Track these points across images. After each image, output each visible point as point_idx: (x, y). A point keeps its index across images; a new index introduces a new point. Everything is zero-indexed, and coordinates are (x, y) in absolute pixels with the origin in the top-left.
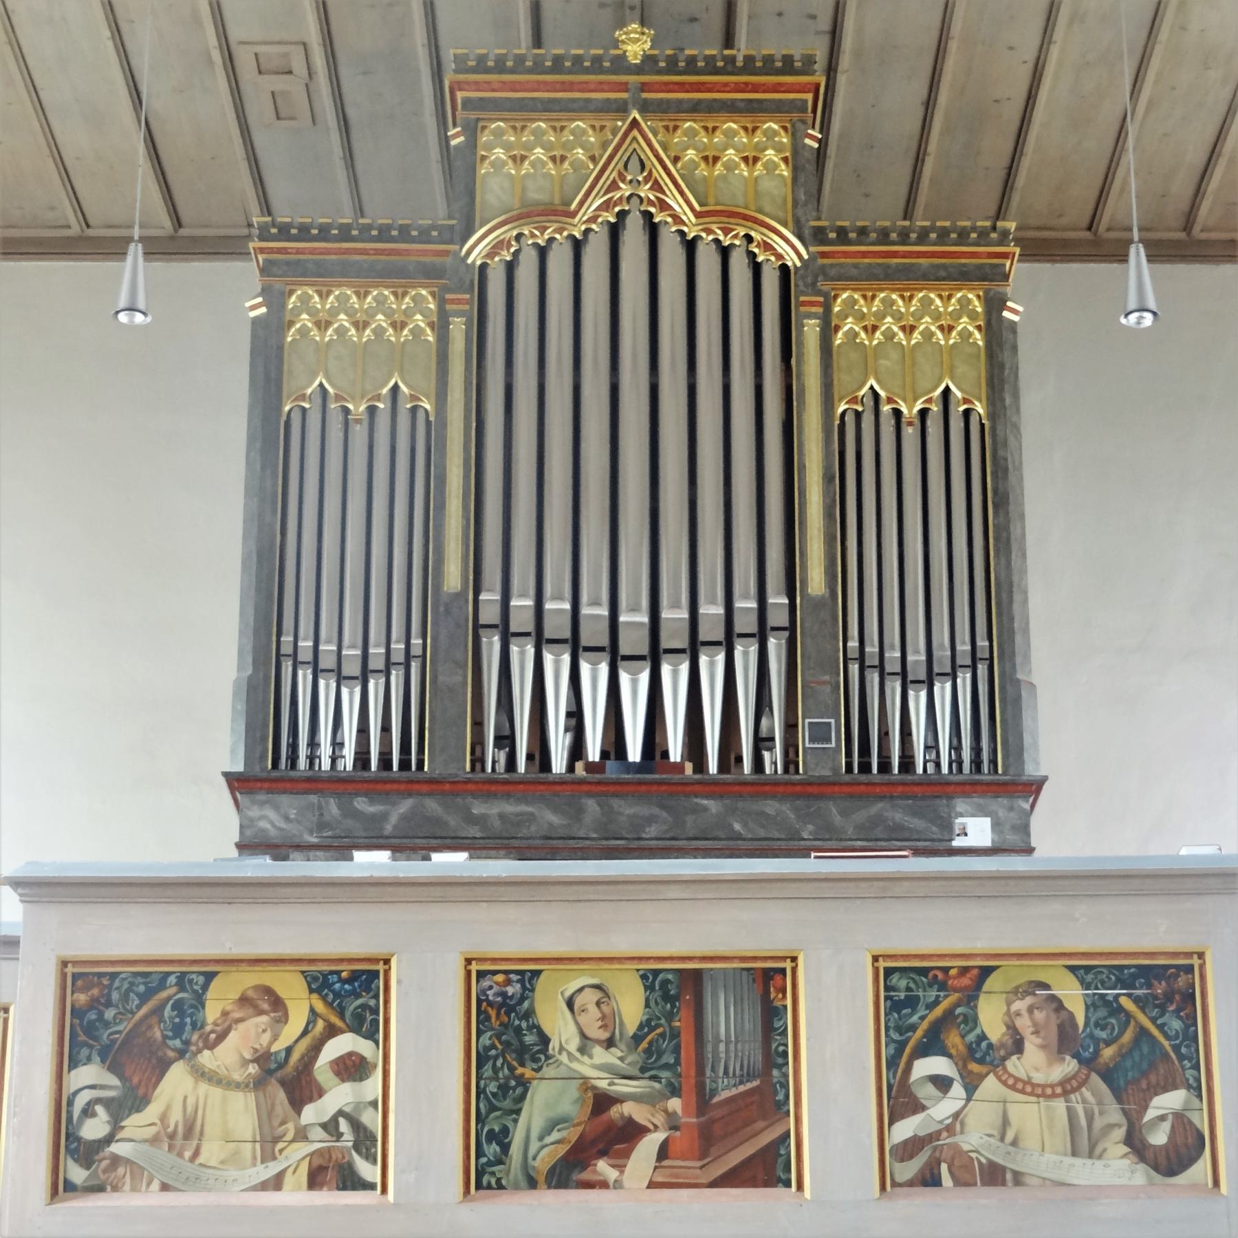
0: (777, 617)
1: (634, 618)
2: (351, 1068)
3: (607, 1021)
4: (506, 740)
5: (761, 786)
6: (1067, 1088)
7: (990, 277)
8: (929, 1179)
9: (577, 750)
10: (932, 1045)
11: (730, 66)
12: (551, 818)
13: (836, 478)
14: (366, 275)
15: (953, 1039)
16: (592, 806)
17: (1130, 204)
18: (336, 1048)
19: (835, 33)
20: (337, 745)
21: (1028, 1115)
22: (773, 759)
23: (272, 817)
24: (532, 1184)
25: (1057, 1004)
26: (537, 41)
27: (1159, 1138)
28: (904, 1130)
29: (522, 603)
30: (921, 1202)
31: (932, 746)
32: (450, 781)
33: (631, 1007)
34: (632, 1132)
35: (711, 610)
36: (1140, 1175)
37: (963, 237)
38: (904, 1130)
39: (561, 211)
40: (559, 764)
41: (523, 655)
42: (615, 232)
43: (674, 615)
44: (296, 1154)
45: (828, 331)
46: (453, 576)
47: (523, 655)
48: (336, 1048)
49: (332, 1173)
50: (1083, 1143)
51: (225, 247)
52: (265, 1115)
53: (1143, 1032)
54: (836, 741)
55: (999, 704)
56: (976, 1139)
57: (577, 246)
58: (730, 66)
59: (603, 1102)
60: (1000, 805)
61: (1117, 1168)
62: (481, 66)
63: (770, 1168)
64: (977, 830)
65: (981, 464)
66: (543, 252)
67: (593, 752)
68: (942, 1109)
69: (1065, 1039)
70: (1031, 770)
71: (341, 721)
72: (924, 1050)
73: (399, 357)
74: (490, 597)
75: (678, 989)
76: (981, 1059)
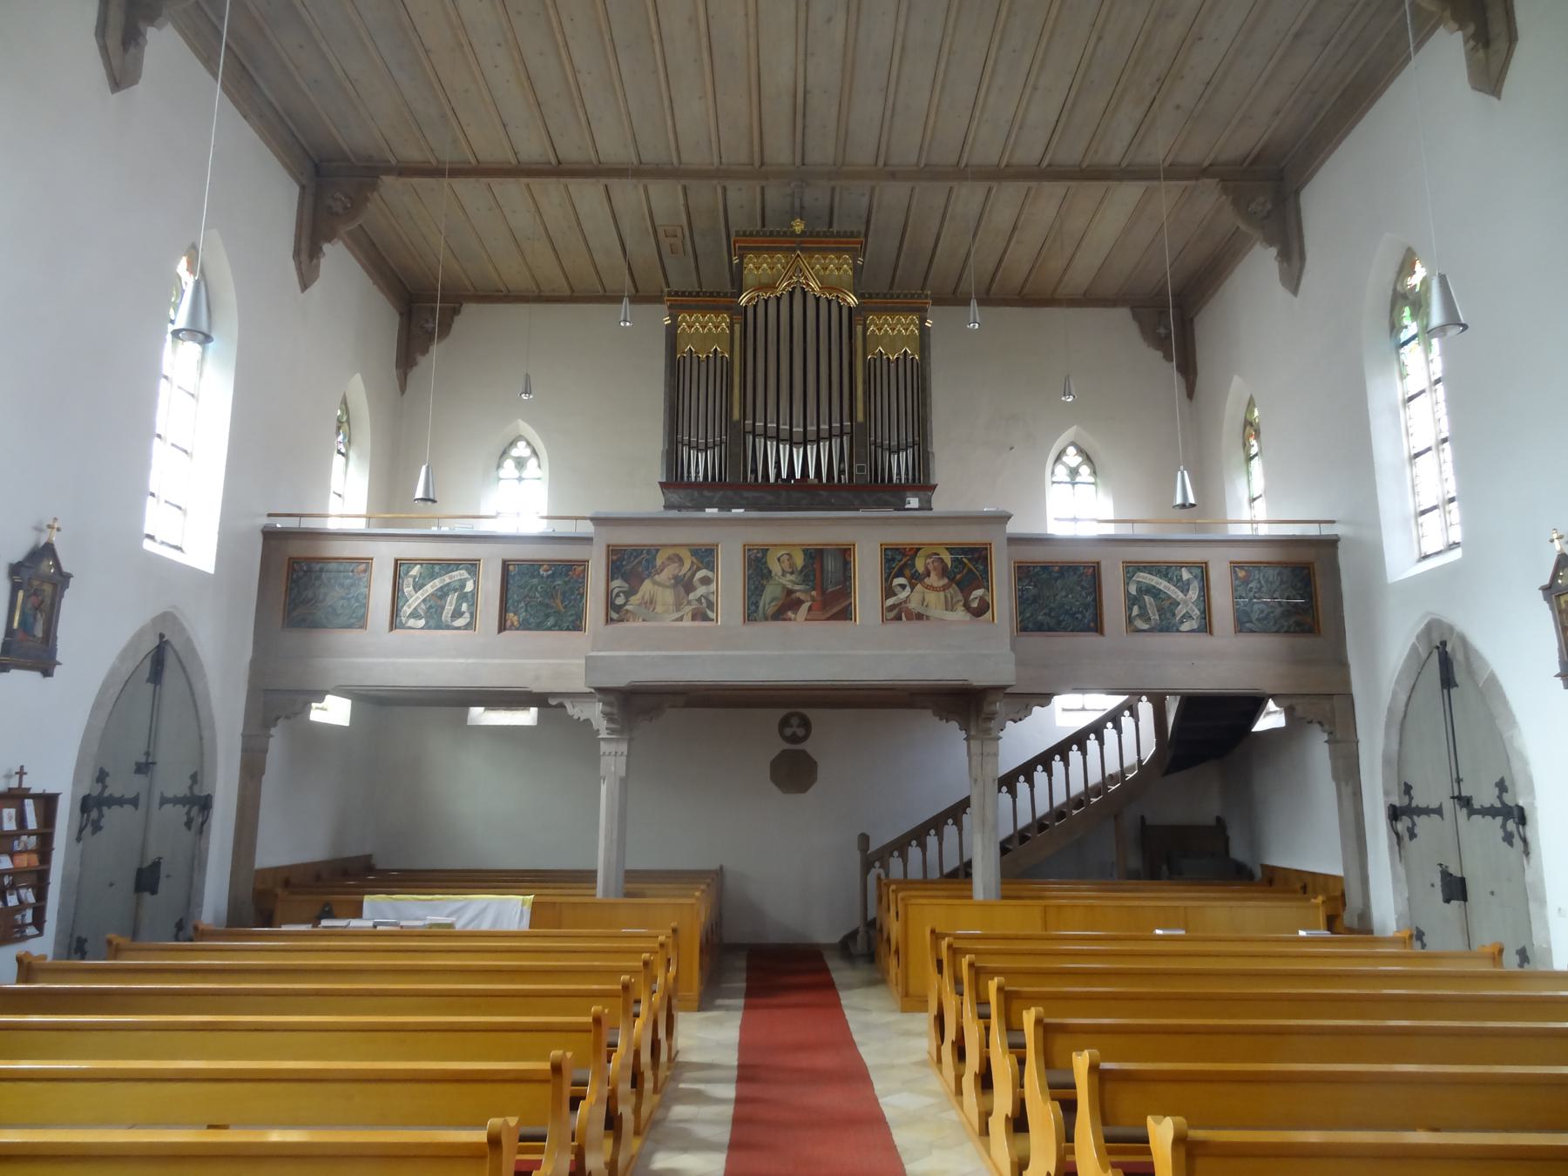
0: (847, 430)
1: (798, 429)
2: (706, 581)
3: (792, 565)
4: (754, 471)
5: (840, 486)
6: (944, 588)
7: (922, 312)
8: (898, 618)
9: (778, 474)
10: (900, 574)
11: (832, 235)
12: (770, 498)
13: (867, 382)
14: (704, 309)
15: (907, 572)
16: (784, 494)
17: (971, 283)
18: (700, 574)
19: (868, 222)
20: (697, 473)
21: (932, 597)
22: (845, 478)
23: (675, 497)
24: (766, 619)
25: (941, 560)
26: (763, 225)
27: (975, 605)
28: (890, 602)
29: (760, 424)
30: (896, 625)
31: (899, 473)
32: (738, 485)
33: (799, 561)
34: (799, 602)
35: (824, 427)
36: (968, 617)
37: (912, 296)
38: (890, 602)
39: (772, 286)
40: (772, 480)
41: (760, 442)
42: (791, 294)
43: (812, 428)
44: (688, 609)
45: (865, 329)
46: (736, 415)
47: (760, 442)
48: (700, 574)
49: (699, 615)
50: (949, 606)
51: (655, 299)
52: (677, 597)
53: (970, 570)
54: (866, 472)
55: (923, 461)
56: (914, 605)
57: (778, 299)
58: (832, 235)
59: (790, 592)
60: (921, 494)
61: (960, 614)
62: (745, 234)
63: (845, 614)
64: (914, 502)
65: (917, 378)
66: (766, 301)
67: (784, 476)
68: (903, 595)
69: (944, 572)
70: (932, 482)
71: (699, 464)
72: (897, 576)
73: (717, 339)
74: (749, 422)
75: (815, 555)
76: (916, 579)
